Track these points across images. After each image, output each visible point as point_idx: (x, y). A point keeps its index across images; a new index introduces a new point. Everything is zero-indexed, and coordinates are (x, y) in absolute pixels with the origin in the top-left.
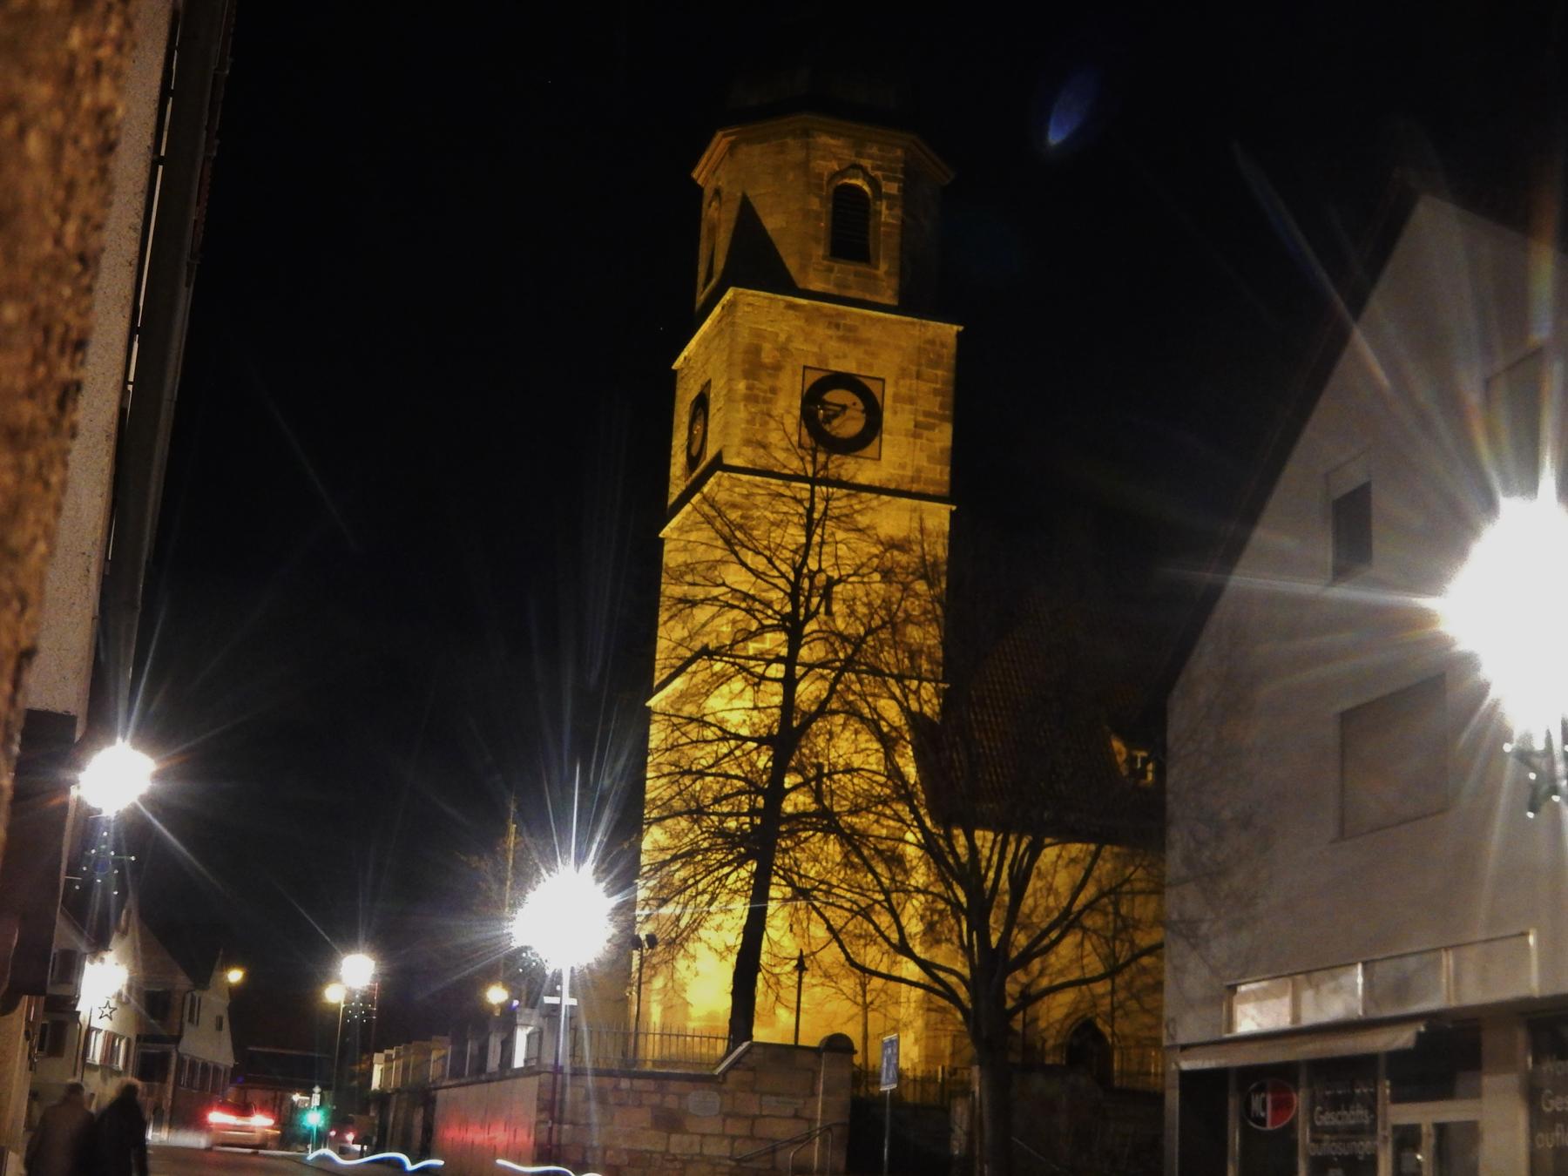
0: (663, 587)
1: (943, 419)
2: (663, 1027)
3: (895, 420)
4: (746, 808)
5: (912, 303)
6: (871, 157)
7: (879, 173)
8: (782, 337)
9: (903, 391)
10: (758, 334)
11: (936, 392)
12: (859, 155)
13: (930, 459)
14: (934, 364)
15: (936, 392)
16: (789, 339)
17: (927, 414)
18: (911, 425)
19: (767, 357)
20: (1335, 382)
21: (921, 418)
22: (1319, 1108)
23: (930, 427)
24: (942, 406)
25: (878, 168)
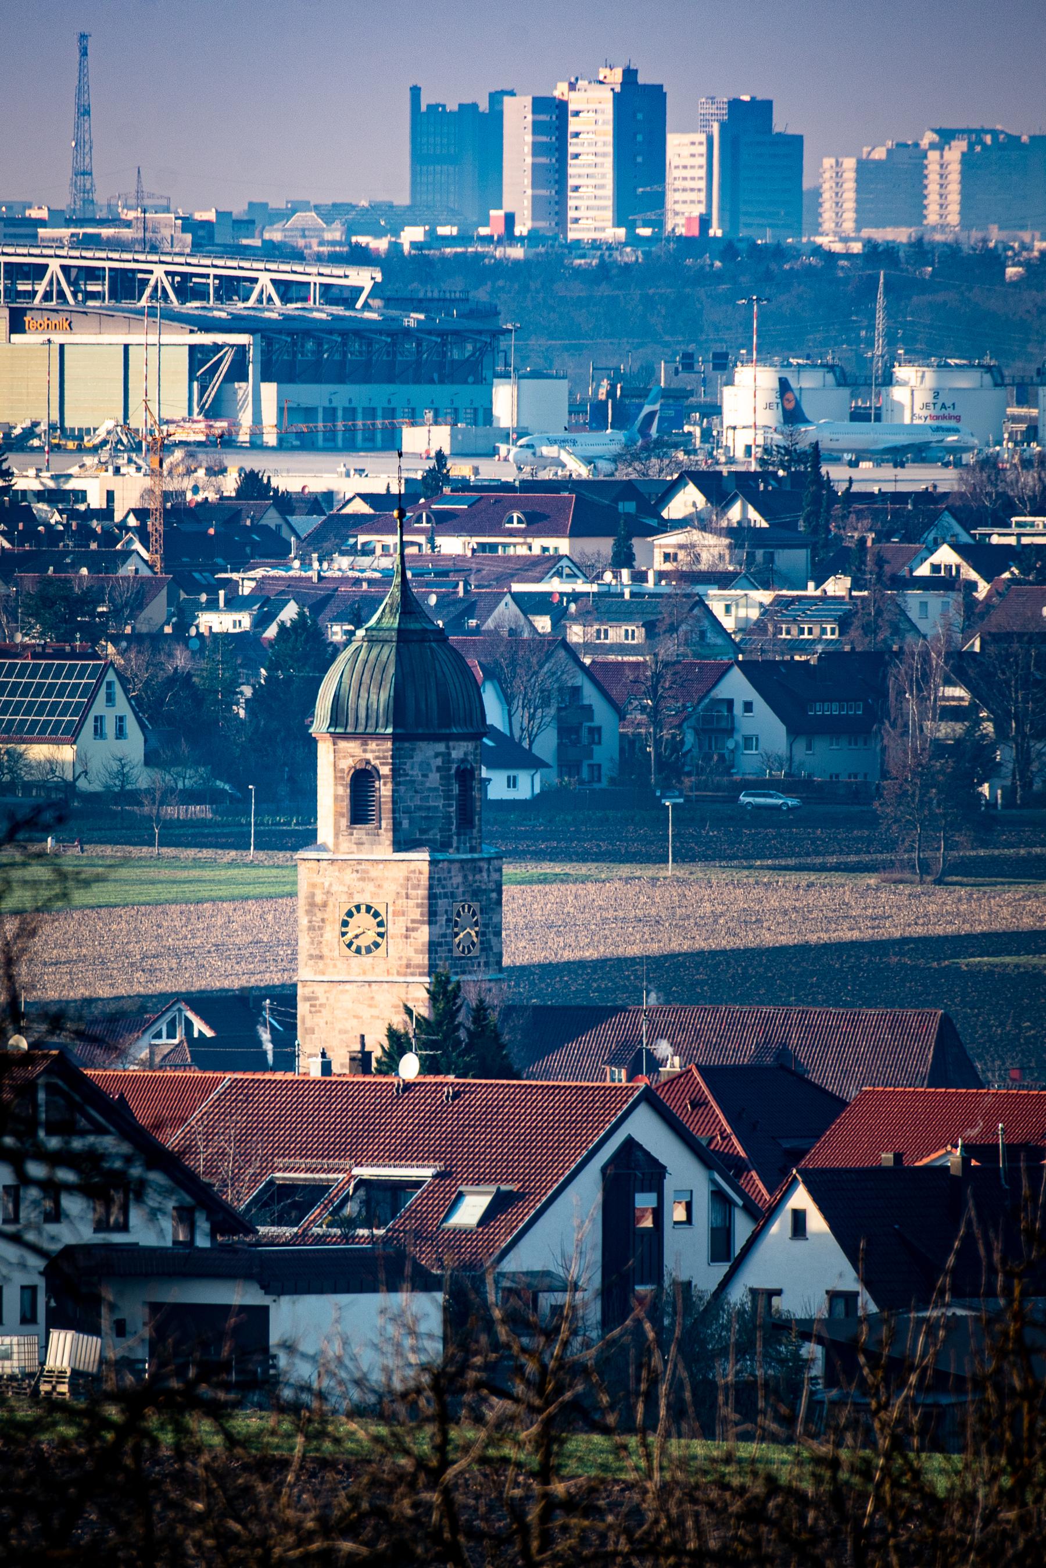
0: (70, 1335)
1: (422, 922)
2: (73, 1371)
3: (395, 927)
4: (723, 459)
5: (401, 844)
6: (373, 751)
7: (377, 762)
8: (327, 884)
9: (398, 908)
10: (314, 885)
11: (418, 906)
12: (365, 751)
13: (416, 951)
14: (416, 887)
15: (418, 906)
16: (331, 885)
17: (413, 921)
18: (404, 931)
19: (319, 899)
20: (295, 1297)
21: (410, 925)
22: (86, 1422)
23: (414, 930)
24: (422, 915)
25: (377, 758)
